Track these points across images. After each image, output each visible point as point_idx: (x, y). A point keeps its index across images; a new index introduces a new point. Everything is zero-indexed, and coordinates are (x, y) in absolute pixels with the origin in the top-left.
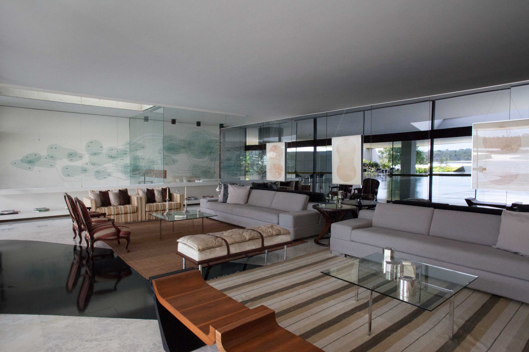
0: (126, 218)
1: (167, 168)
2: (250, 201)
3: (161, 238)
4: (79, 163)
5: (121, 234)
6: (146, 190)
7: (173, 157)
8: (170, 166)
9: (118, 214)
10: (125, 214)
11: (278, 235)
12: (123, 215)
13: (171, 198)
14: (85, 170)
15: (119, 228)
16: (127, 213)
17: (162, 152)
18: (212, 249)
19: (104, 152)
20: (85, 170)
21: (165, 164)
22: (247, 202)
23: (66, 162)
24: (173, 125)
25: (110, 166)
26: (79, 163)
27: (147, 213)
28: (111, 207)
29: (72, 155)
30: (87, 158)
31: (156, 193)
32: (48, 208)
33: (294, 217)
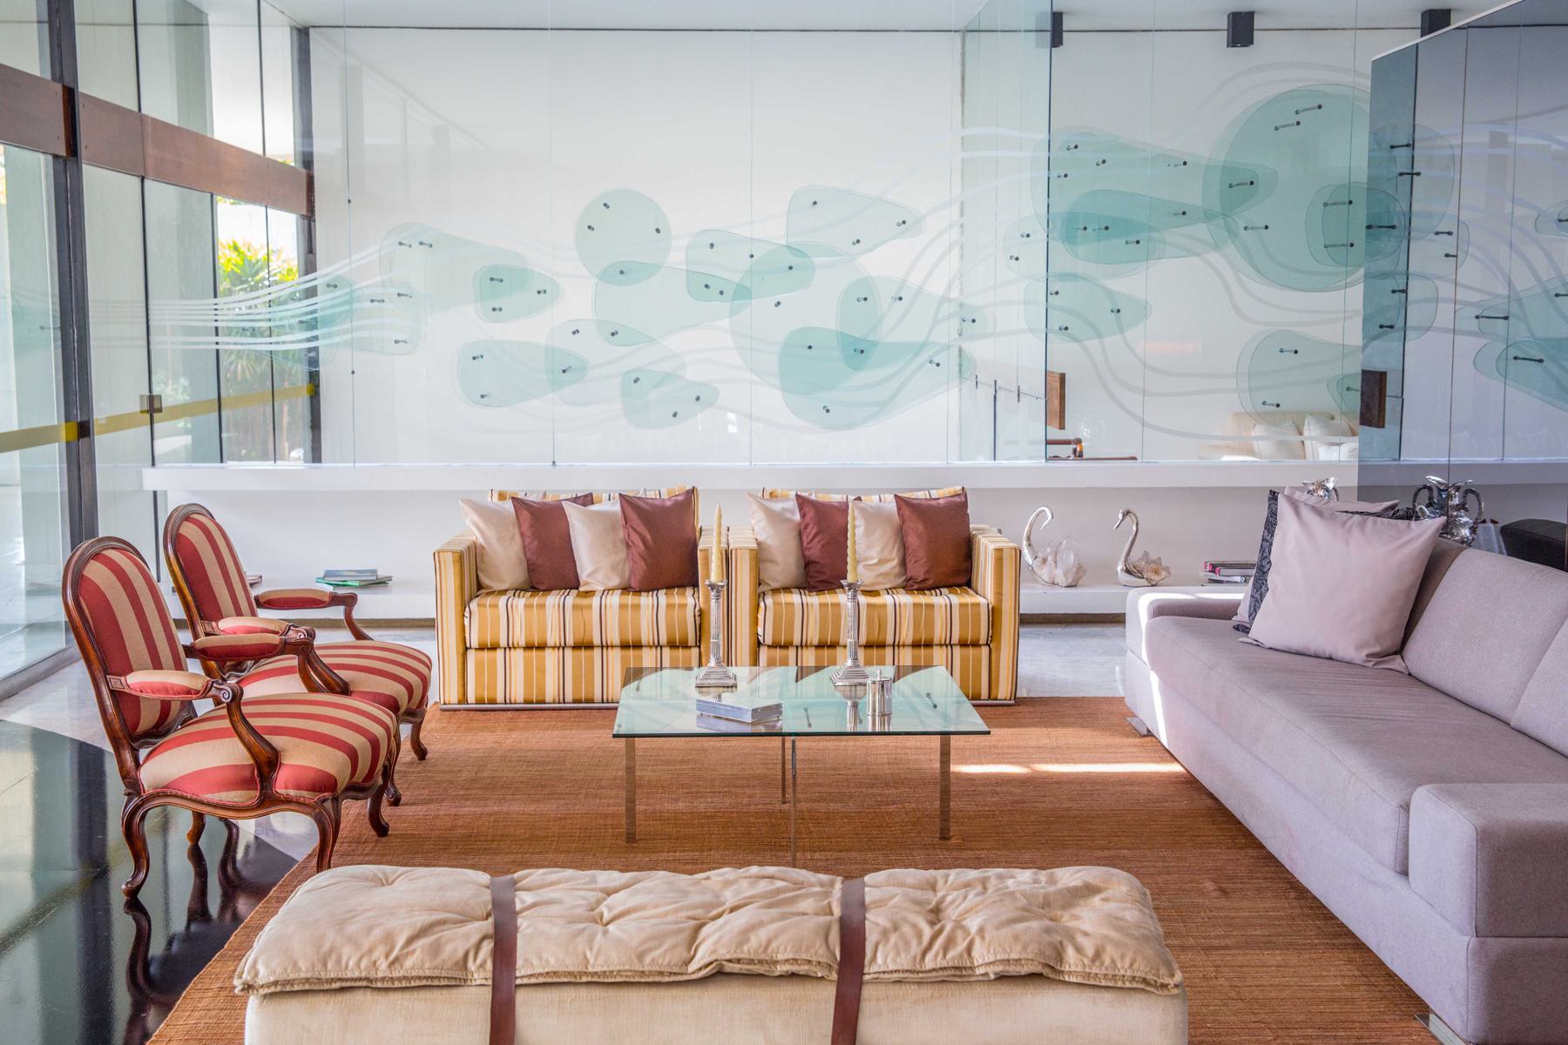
0: (534, 675)
1: (1066, 357)
2: (1424, 654)
3: (631, 838)
4: (531, 329)
5: (282, 783)
6: (890, 504)
7: (1114, 285)
8: (1093, 345)
9: (584, 646)
10: (529, 647)
11: (1034, 977)
12: (518, 656)
13: (960, 574)
14: (567, 371)
15: (277, 741)
16: (542, 647)
17: (1034, 254)
18: (359, 997)
19: (676, 258)
20: (567, 371)
21: (1055, 329)
22: (1400, 650)
23: (466, 324)
24: (1239, 51)
25: (705, 346)
26: (531, 329)
27: (471, 655)
28: (843, 598)
29: (500, 283)
30: (578, 299)
31: (858, 531)
32: (382, 573)
33: (1485, 837)
